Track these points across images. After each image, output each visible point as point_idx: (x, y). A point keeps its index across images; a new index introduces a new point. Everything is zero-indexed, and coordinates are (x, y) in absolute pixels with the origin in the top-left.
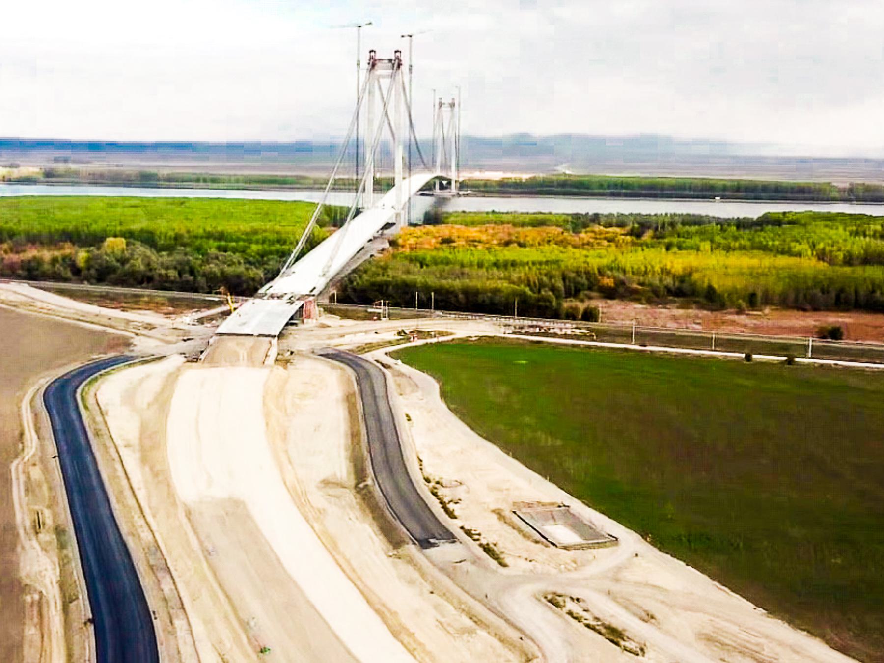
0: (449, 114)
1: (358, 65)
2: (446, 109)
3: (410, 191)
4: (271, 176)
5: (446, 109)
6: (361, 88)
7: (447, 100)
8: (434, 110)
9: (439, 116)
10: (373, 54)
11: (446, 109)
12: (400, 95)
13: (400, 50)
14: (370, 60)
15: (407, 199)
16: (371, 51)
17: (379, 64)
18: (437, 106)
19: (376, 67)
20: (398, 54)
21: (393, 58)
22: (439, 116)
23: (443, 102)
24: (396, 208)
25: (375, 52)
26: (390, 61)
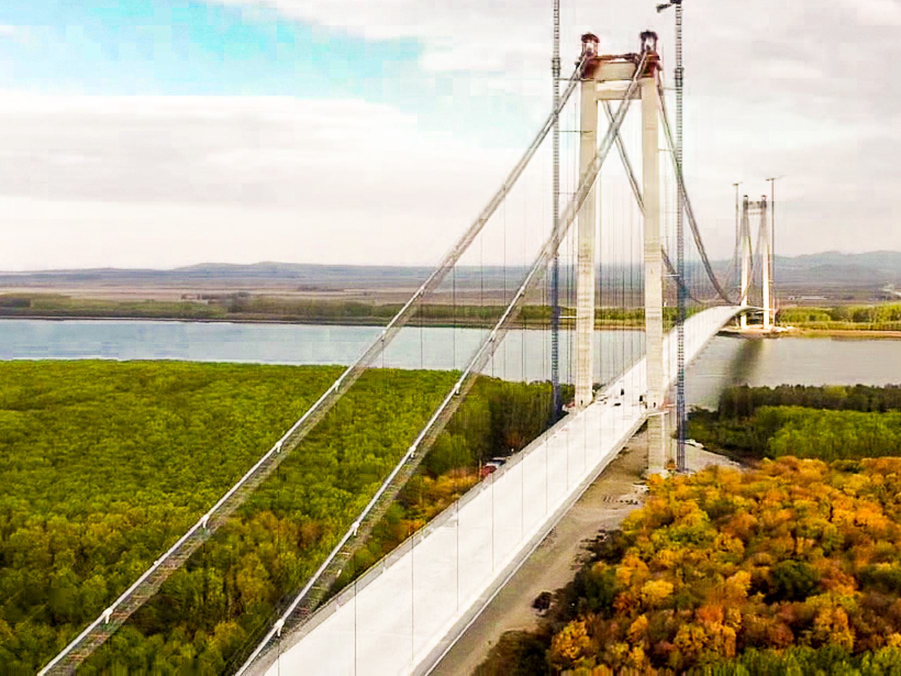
0: (758, 218)
1: (556, 70)
2: (754, 211)
3: (681, 358)
4: (18, 294)
5: (754, 211)
6: (564, 200)
7: (755, 197)
8: (737, 215)
9: (745, 220)
10: (590, 45)
11: (753, 211)
12: (654, 129)
13: (651, 30)
14: (583, 55)
15: (674, 374)
16: (587, 38)
17: (605, 69)
18: (741, 208)
19: (598, 76)
20: (649, 42)
21: (638, 51)
22: (745, 220)
23: (750, 200)
24: (650, 401)
25: (597, 41)
26: (630, 57)
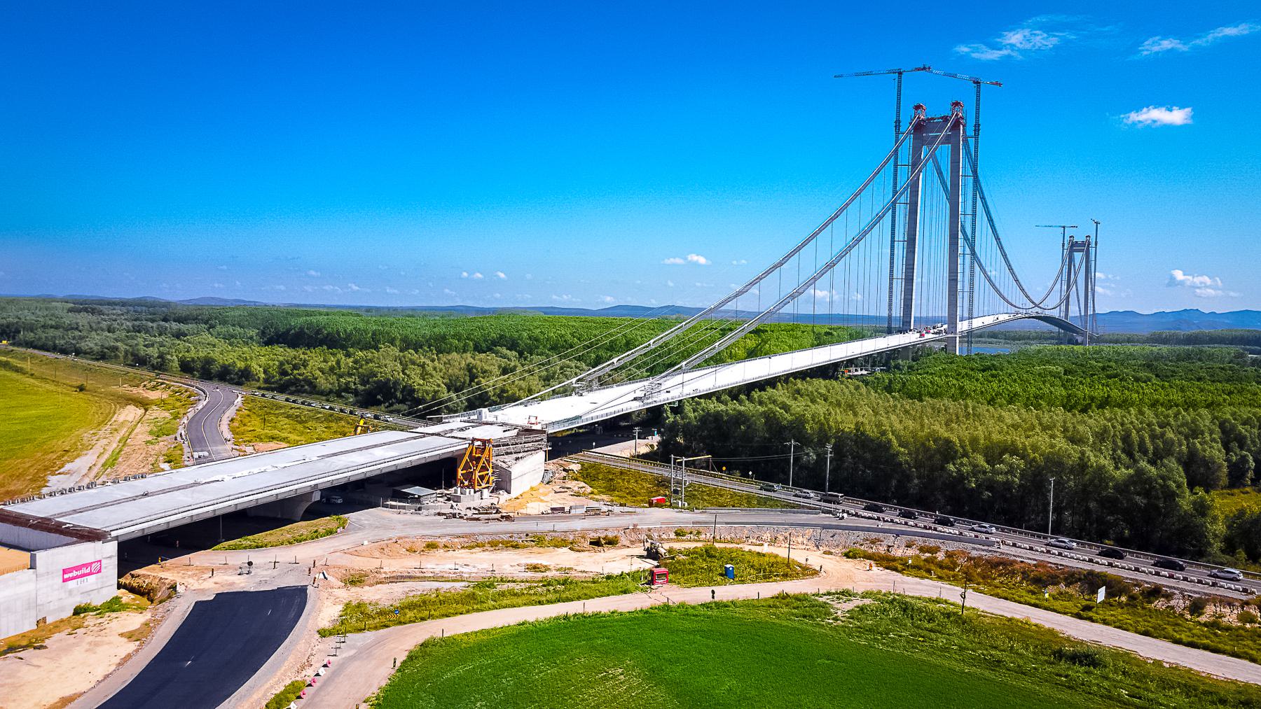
20: (1088, 238)
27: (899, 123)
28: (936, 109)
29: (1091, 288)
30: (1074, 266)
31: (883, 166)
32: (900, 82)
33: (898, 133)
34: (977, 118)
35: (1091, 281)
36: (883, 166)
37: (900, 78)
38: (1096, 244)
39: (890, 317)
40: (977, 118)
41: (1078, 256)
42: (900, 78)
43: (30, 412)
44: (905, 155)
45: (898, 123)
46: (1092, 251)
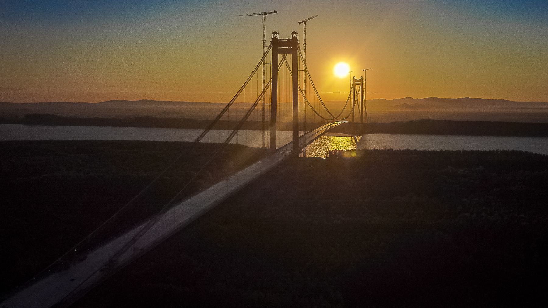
20: (362, 78)
27: (265, 41)
28: (285, 35)
29: (364, 100)
30: (356, 91)
31: (254, 72)
32: (265, 19)
33: (265, 46)
34: (305, 40)
35: (364, 97)
36: (254, 72)
37: (265, 17)
38: (365, 81)
39: (264, 121)
40: (305, 40)
41: (358, 86)
42: (265, 17)
43: (138, 195)
44: (269, 58)
45: (264, 40)
46: (364, 84)
